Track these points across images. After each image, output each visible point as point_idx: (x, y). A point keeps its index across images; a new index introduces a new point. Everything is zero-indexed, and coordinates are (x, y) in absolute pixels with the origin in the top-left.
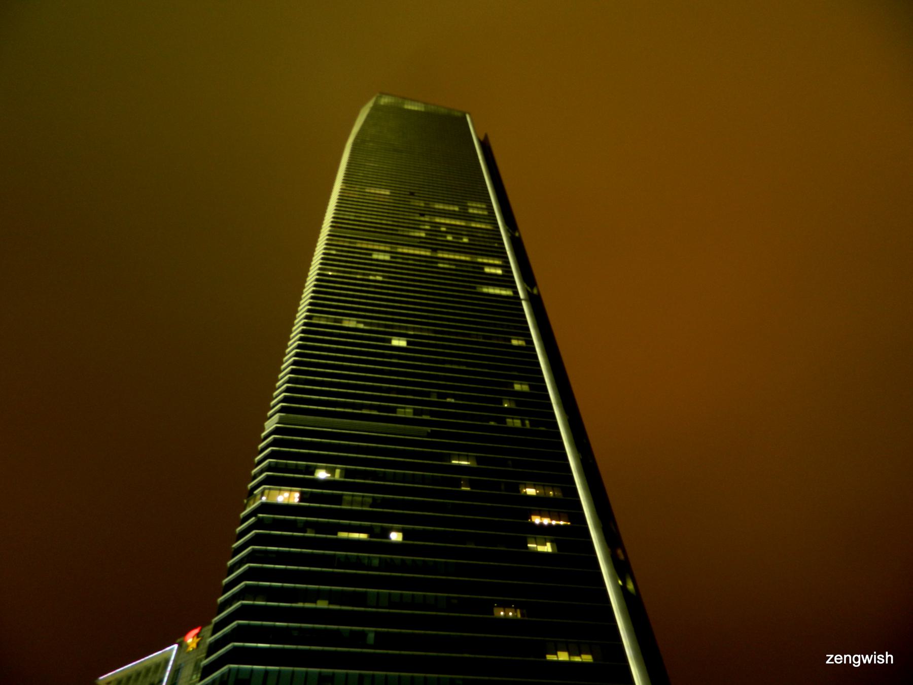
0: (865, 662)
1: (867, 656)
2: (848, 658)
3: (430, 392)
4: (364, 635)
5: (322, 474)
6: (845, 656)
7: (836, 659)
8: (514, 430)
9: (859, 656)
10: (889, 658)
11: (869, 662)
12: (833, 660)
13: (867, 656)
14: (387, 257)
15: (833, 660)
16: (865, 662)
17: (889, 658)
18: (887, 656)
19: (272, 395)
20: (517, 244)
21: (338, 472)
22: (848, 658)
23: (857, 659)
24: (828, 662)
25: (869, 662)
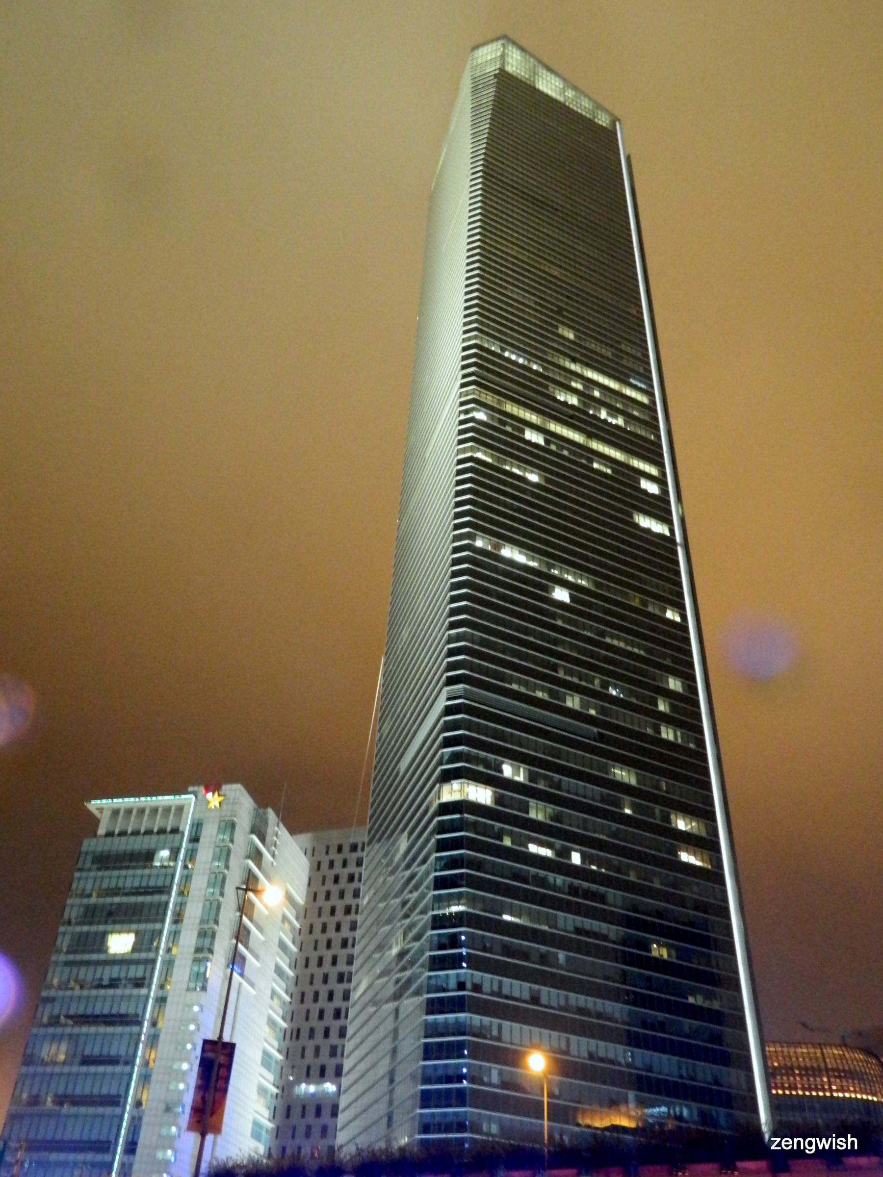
0: (821, 1147)
1: (824, 1140)
2: (799, 1142)
3: (480, 645)
4: (99, 896)
5: (658, 951)
6: (796, 1140)
7: (783, 1143)
8: (666, 743)
9: (813, 1140)
10: (853, 1142)
11: (827, 1147)
12: (779, 1145)
13: (824, 1140)
14: (573, 400)
15: (779, 1145)
16: (821, 1147)
17: (853, 1142)
18: (850, 1140)
19: (187, 788)
20: (683, 521)
21: (495, 1078)
22: (799, 1142)
23: (810, 1144)
24: (773, 1148)
25: (827, 1147)
